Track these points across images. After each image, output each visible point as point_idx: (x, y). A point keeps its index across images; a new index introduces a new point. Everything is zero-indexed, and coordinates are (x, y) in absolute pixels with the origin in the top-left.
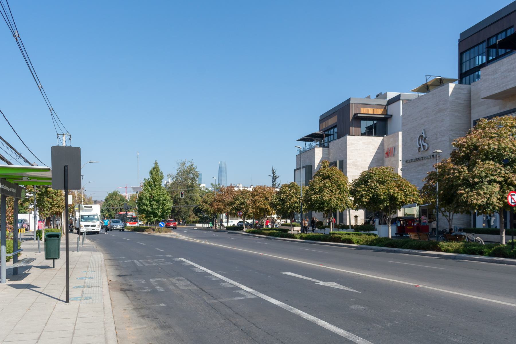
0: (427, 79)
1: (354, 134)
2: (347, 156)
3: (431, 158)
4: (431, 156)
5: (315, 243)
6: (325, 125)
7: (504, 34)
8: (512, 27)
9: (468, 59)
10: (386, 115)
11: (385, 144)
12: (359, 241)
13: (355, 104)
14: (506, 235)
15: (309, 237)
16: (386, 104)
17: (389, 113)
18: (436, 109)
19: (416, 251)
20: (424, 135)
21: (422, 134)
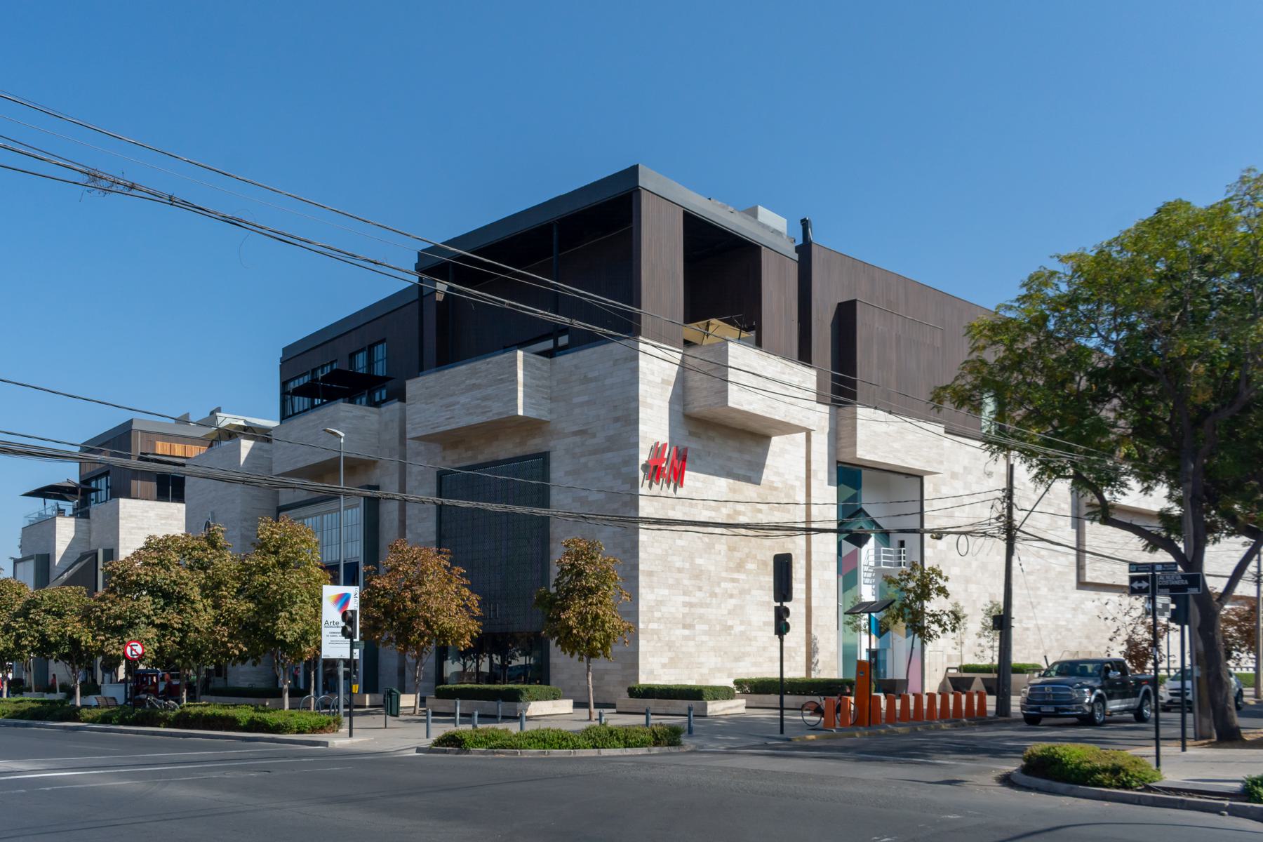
2: (120, 541)
8: (336, 361)
13: (142, 431)
14: (290, 696)
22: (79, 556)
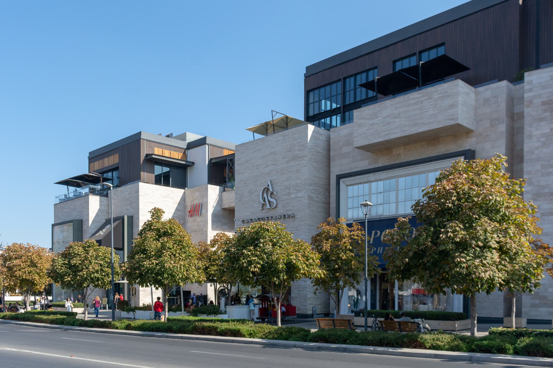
0: (273, 116)
1: (146, 181)
3: (281, 218)
4: (281, 216)
5: (167, 337)
6: (97, 165)
7: (364, 75)
8: (443, 44)
9: (317, 99)
10: (186, 161)
11: (187, 199)
12: (252, 332)
13: (147, 140)
15: (144, 326)
16: (185, 147)
17: (190, 159)
18: (288, 155)
19: (390, 350)
20: (270, 188)
21: (268, 186)
22: (104, 221)
